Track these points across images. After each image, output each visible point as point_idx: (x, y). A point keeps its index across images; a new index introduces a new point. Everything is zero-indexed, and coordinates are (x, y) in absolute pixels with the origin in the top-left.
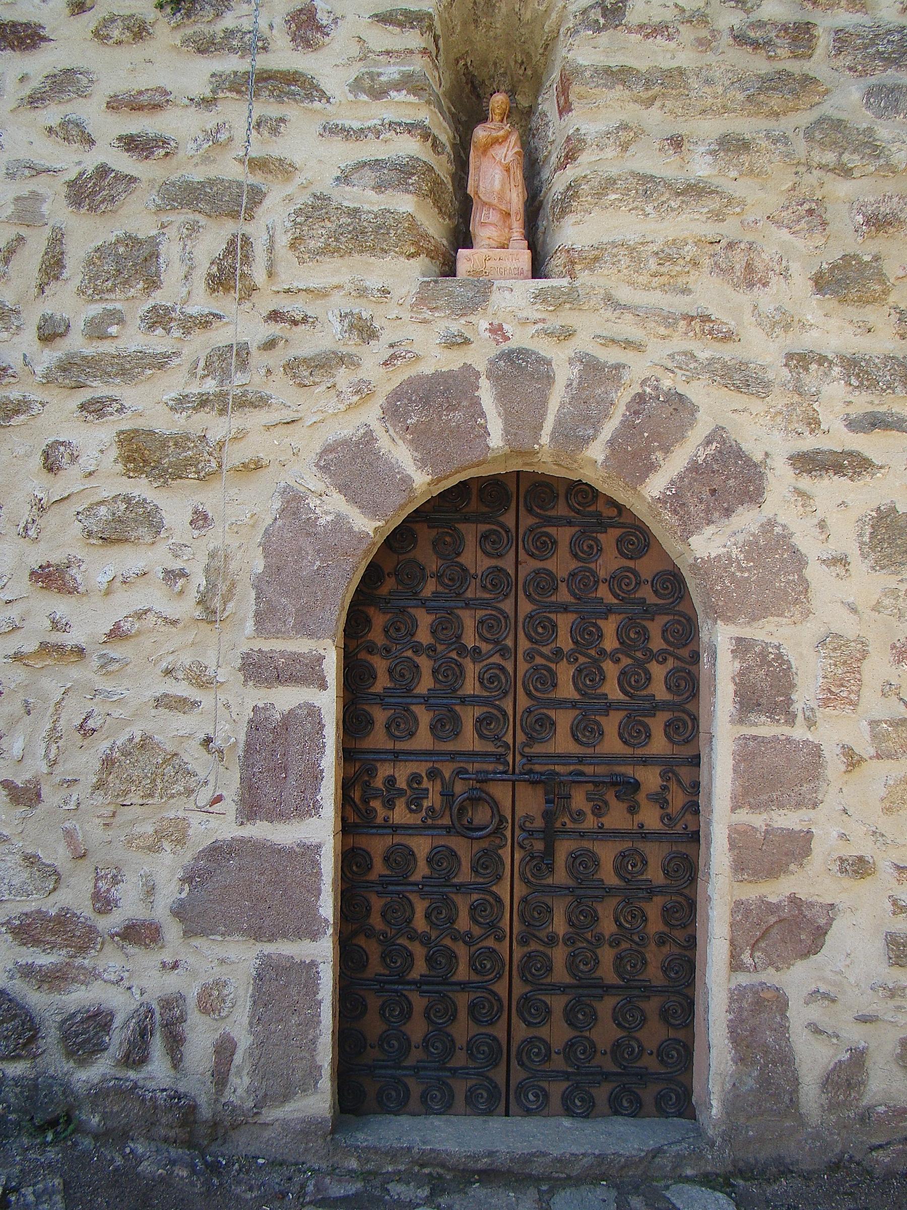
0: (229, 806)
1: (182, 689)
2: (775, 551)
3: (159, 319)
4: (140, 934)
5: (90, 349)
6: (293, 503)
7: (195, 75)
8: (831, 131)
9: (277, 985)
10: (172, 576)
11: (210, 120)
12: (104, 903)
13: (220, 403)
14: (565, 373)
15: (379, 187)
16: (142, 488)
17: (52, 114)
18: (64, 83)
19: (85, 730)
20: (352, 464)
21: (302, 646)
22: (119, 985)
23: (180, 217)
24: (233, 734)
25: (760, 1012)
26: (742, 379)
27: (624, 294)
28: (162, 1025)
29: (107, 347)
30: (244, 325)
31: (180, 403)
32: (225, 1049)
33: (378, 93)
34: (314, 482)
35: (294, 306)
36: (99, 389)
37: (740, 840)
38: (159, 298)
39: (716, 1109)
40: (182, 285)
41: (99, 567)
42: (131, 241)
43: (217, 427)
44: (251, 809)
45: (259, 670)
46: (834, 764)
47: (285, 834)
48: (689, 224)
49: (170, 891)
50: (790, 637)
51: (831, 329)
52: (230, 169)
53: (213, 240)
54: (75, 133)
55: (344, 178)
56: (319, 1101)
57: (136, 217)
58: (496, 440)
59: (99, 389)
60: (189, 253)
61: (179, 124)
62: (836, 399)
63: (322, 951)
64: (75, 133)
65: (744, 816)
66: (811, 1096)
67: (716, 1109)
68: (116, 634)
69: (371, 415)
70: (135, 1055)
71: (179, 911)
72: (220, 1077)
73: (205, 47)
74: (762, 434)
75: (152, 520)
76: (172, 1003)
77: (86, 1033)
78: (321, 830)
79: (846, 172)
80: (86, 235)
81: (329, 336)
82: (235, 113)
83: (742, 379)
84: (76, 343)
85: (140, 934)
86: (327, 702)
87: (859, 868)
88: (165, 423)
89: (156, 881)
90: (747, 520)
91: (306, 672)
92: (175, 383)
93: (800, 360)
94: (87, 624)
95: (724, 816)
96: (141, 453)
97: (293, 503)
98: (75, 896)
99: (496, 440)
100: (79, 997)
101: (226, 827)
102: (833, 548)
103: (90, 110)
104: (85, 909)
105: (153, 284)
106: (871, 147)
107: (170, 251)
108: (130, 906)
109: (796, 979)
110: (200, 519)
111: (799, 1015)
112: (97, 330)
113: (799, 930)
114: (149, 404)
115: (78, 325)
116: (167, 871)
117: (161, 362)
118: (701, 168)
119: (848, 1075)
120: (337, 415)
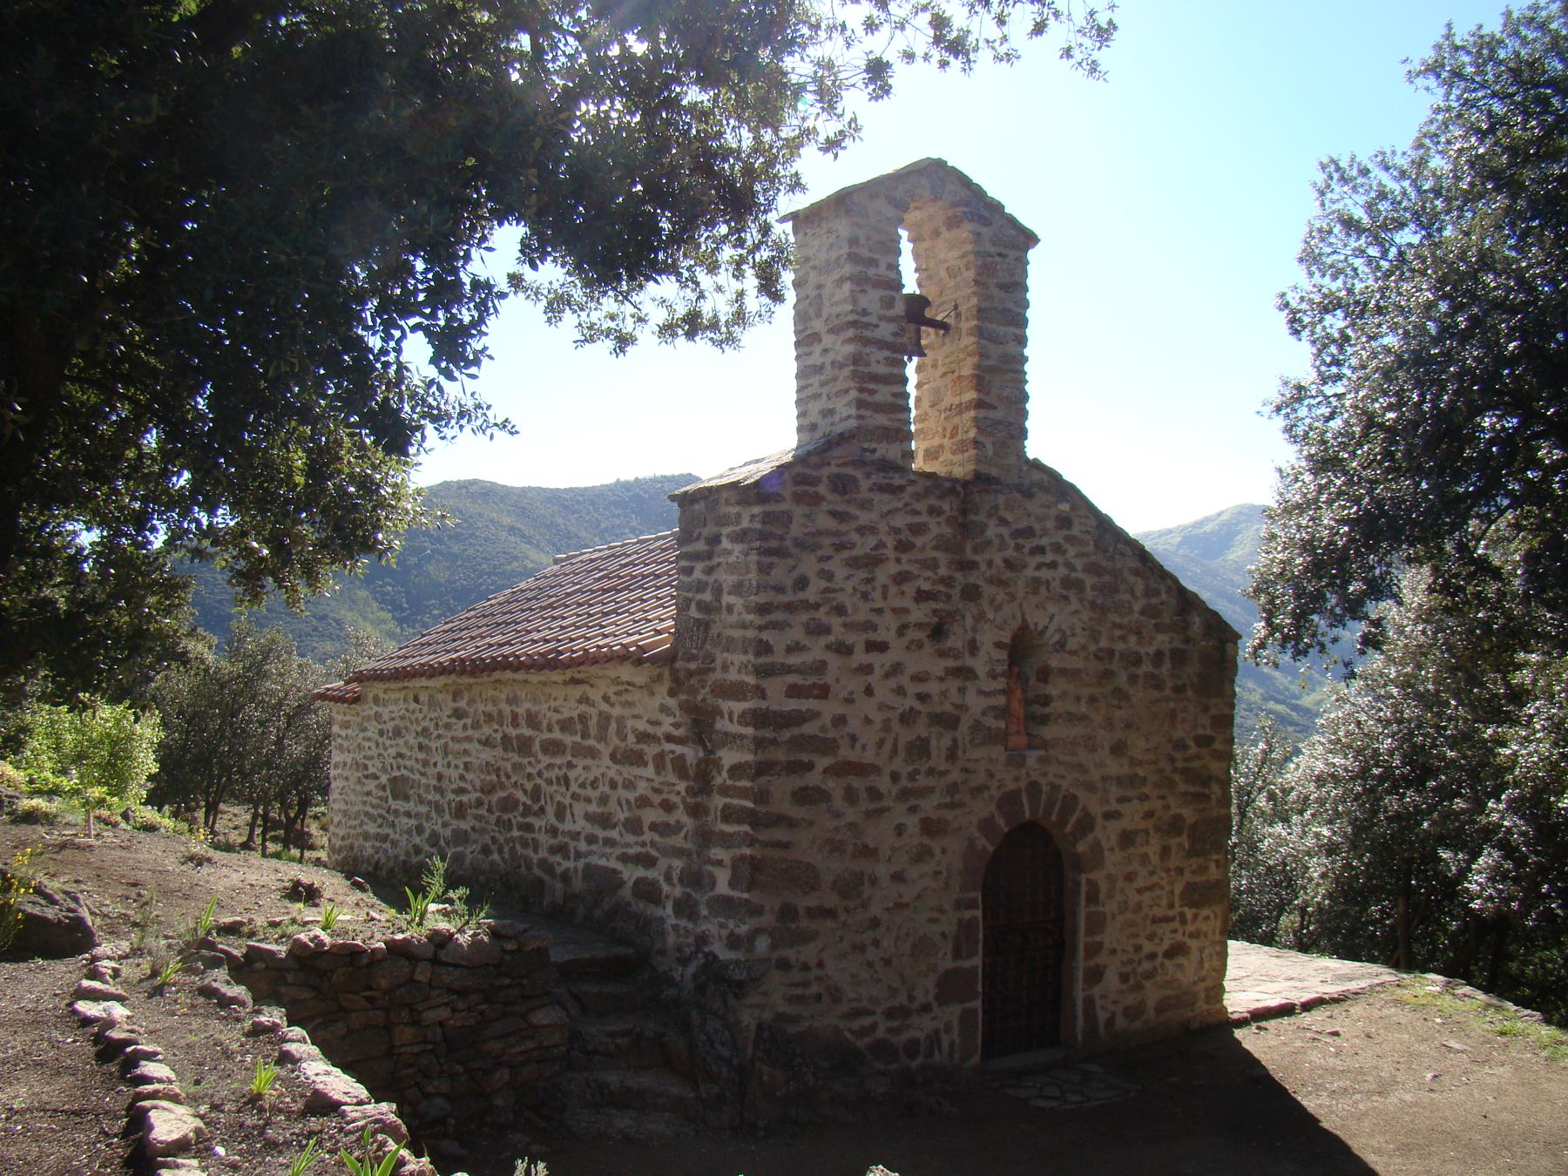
0: (949, 956)
1: (935, 915)
2: (1097, 847)
3: (931, 772)
4: (926, 1008)
5: (910, 785)
6: (971, 842)
7: (938, 666)
8: (1118, 692)
9: (966, 1019)
10: (936, 873)
11: (943, 687)
12: (911, 998)
13: (952, 806)
14: (1045, 789)
15: (996, 718)
16: (926, 840)
17: (892, 683)
18: (896, 669)
19: (907, 935)
20: (987, 826)
21: (972, 895)
22: (920, 1028)
23: (936, 729)
24: (951, 929)
25: (1089, 1002)
26: (1090, 787)
27: (1062, 758)
28: (934, 1039)
29: (915, 785)
30: (955, 776)
31: (939, 807)
32: (952, 1044)
33: (994, 678)
34: (977, 834)
35: (970, 766)
36: (913, 802)
37: (1086, 945)
38: (931, 764)
39: (1080, 1037)
40: (938, 760)
41: (913, 872)
42: (919, 738)
43: (949, 815)
44: (957, 954)
45: (959, 905)
46: (1109, 917)
47: (967, 964)
48: (1079, 730)
49: (933, 990)
50: (1098, 876)
51: (1114, 767)
52: (948, 708)
53: (946, 741)
54: (901, 691)
55: (984, 713)
56: (976, 1059)
57: (921, 729)
58: (1027, 815)
59: (913, 802)
60: (940, 743)
61: (933, 687)
62: (1114, 791)
63: (978, 1004)
64: (901, 691)
65: (1090, 940)
66: (1102, 1029)
67: (1080, 1037)
68: (919, 897)
69: (993, 808)
70: (930, 1054)
71: (937, 997)
72: (951, 1054)
73: (942, 654)
74: (1096, 809)
75: (930, 853)
76: (937, 1031)
77: (912, 1048)
78: (977, 961)
79: (1120, 707)
80: (906, 736)
81: (978, 779)
82: (953, 685)
83: (1090, 787)
84: (904, 782)
85: (926, 1008)
86: (979, 913)
87: (1113, 951)
88: (934, 815)
89: (927, 988)
90: (1090, 837)
91: (972, 905)
92: (936, 799)
93: (1105, 779)
94: (908, 893)
95: (1082, 939)
96: (929, 827)
97: (971, 842)
98: (902, 999)
99: (1027, 815)
100: (905, 1036)
101: (948, 964)
102: (1131, 949)
103: (904, 680)
104: (905, 1002)
105: (929, 758)
106: (1127, 698)
107: (934, 743)
108: (920, 998)
109: (1097, 991)
110: (944, 851)
111: (1099, 1003)
112: (912, 776)
113: (1095, 975)
114: (928, 806)
115: (904, 775)
116: (930, 983)
117: (931, 790)
118: (1083, 708)
119: (1110, 1022)
120: (982, 808)
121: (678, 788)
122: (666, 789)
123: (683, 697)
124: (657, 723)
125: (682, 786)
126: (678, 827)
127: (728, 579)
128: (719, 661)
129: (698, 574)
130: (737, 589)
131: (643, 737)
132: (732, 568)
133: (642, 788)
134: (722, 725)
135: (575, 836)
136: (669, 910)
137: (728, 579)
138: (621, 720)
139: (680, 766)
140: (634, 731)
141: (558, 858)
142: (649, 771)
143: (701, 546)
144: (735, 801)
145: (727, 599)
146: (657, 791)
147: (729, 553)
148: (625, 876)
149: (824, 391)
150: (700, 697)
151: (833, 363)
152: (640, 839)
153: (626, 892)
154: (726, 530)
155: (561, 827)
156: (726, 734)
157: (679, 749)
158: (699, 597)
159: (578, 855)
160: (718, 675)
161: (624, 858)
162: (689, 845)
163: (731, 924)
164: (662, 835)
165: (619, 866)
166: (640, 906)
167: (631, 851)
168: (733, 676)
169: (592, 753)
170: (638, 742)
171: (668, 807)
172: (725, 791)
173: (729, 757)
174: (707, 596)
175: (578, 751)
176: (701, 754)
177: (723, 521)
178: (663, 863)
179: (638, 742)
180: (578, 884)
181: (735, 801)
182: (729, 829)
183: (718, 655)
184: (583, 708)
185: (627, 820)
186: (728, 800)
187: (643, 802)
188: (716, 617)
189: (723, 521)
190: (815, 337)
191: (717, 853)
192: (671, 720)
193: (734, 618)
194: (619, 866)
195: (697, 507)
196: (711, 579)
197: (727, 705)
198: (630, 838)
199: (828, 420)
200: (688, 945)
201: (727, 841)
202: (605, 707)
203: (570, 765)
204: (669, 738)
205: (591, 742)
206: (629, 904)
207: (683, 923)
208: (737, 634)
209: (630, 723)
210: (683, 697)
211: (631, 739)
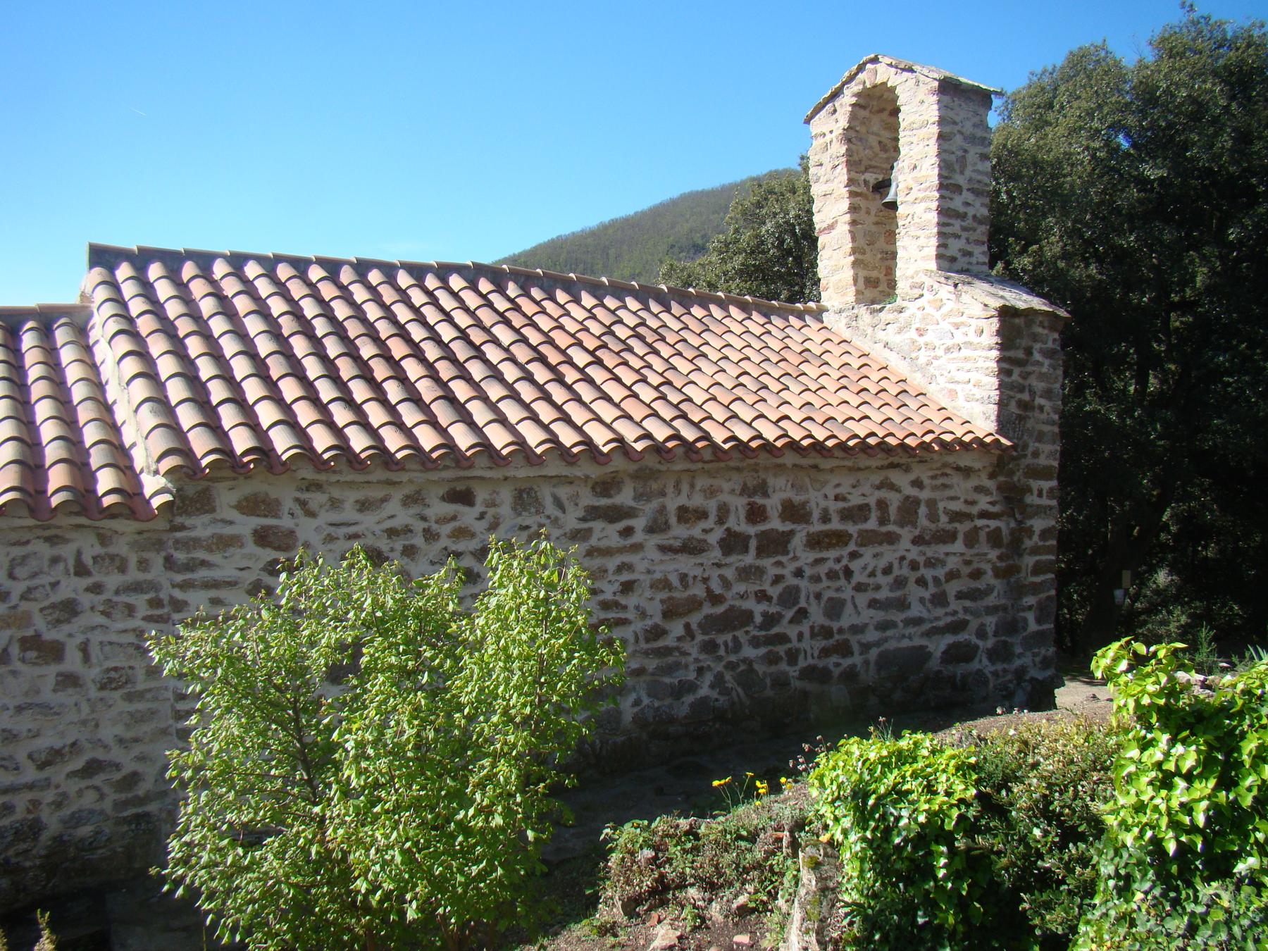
53: (731, 523)
121: (990, 556)
122: (976, 559)
123: (1001, 479)
124: (973, 503)
125: (993, 554)
126: (990, 589)
127: (1039, 386)
128: (1030, 449)
129: (1015, 377)
130: (1048, 394)
131: (956, 517)
132: (1042, 376)
133: (952, 563)
134: (1031, 499)
135: (857, 629)
136: (985, 661)
137: (1039, 386)
138: (932, 504)
139: (995, 538)
140: (946, 512)
141: (834, 659)
142: (958, 546)
143: (1020, 354)
144: (1044, 557)
145: (1039, 401)
146: (968, 563)
147: (1041, 364)
148: (931, 648)
149: (965, 234)
150: (1015, 479)
151: (974, 217)
152: (949, 610)
153: (934, 664)
154: (1037, 346)
155: (835, 626)
156: (1038, 506)
157: (993, 524)
158: (1019, 396)
159: (866, 647)
160: (1029, 460)
161: (928, 634)
162: (1003, 601)
163: (1043, 651)
164: (974, 599)
165: (924, 642)
166: (961, 669)
167: (941, 623)
168: (1042, 461)
169: (891, 539)
170: (951, 521)
171: (977, 575)
172: (1035, 551)
173: (1038, 524)
174: (1025, 397)
175: (868, 539)
176: (1013, 525)
177: (1035, 338)
178: (974, 624)
179: (951, 521)
180: (869, 676)
181: (1044, 557)
182: (1038, 579)
183: (1031, 444)
184: (883, 494)
185: (933, 596)
186: (1038, 558)
187: (952, 575)
188: (1030, 414)
189: (1035, 338)
190: (958, 189)
191: (1030, 600)
192: (989, 499)
193: (1044, 416)
194: (924, 642)
195: (1017, 321)
196: (1026, 383)
197: (1035, 484)
198: (939, 612)
199: (966, 259)
200: (1010, 681)
201: (1035, 589)
202: (913, 492)
203: (854, 555)
204: (984, 515)
205: (891, 528)
206: (940, 672)
207: (999, 667)
208: (1046, 428)
209: (941, 505)
210: (1001, 479)
211: (944, 519)
